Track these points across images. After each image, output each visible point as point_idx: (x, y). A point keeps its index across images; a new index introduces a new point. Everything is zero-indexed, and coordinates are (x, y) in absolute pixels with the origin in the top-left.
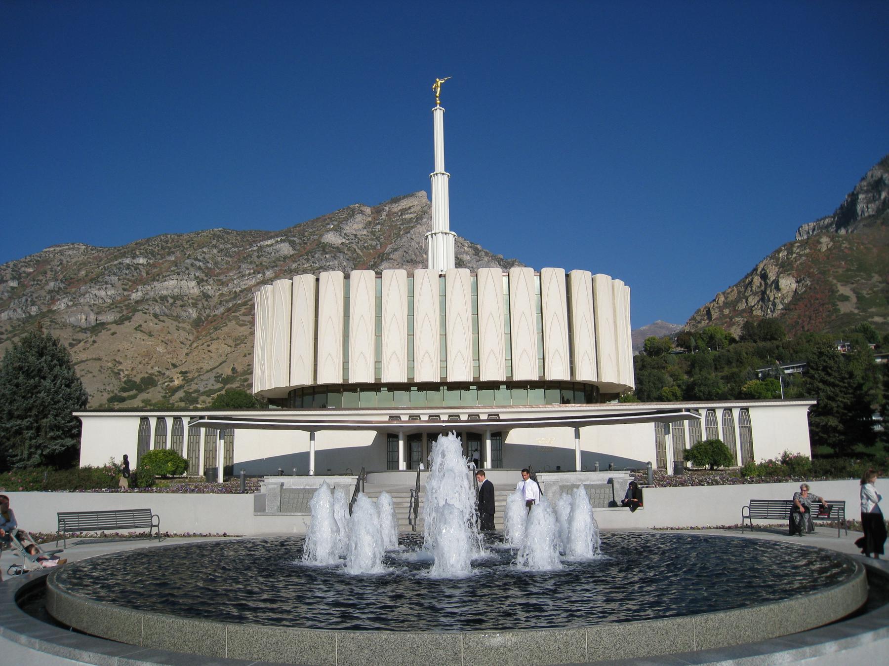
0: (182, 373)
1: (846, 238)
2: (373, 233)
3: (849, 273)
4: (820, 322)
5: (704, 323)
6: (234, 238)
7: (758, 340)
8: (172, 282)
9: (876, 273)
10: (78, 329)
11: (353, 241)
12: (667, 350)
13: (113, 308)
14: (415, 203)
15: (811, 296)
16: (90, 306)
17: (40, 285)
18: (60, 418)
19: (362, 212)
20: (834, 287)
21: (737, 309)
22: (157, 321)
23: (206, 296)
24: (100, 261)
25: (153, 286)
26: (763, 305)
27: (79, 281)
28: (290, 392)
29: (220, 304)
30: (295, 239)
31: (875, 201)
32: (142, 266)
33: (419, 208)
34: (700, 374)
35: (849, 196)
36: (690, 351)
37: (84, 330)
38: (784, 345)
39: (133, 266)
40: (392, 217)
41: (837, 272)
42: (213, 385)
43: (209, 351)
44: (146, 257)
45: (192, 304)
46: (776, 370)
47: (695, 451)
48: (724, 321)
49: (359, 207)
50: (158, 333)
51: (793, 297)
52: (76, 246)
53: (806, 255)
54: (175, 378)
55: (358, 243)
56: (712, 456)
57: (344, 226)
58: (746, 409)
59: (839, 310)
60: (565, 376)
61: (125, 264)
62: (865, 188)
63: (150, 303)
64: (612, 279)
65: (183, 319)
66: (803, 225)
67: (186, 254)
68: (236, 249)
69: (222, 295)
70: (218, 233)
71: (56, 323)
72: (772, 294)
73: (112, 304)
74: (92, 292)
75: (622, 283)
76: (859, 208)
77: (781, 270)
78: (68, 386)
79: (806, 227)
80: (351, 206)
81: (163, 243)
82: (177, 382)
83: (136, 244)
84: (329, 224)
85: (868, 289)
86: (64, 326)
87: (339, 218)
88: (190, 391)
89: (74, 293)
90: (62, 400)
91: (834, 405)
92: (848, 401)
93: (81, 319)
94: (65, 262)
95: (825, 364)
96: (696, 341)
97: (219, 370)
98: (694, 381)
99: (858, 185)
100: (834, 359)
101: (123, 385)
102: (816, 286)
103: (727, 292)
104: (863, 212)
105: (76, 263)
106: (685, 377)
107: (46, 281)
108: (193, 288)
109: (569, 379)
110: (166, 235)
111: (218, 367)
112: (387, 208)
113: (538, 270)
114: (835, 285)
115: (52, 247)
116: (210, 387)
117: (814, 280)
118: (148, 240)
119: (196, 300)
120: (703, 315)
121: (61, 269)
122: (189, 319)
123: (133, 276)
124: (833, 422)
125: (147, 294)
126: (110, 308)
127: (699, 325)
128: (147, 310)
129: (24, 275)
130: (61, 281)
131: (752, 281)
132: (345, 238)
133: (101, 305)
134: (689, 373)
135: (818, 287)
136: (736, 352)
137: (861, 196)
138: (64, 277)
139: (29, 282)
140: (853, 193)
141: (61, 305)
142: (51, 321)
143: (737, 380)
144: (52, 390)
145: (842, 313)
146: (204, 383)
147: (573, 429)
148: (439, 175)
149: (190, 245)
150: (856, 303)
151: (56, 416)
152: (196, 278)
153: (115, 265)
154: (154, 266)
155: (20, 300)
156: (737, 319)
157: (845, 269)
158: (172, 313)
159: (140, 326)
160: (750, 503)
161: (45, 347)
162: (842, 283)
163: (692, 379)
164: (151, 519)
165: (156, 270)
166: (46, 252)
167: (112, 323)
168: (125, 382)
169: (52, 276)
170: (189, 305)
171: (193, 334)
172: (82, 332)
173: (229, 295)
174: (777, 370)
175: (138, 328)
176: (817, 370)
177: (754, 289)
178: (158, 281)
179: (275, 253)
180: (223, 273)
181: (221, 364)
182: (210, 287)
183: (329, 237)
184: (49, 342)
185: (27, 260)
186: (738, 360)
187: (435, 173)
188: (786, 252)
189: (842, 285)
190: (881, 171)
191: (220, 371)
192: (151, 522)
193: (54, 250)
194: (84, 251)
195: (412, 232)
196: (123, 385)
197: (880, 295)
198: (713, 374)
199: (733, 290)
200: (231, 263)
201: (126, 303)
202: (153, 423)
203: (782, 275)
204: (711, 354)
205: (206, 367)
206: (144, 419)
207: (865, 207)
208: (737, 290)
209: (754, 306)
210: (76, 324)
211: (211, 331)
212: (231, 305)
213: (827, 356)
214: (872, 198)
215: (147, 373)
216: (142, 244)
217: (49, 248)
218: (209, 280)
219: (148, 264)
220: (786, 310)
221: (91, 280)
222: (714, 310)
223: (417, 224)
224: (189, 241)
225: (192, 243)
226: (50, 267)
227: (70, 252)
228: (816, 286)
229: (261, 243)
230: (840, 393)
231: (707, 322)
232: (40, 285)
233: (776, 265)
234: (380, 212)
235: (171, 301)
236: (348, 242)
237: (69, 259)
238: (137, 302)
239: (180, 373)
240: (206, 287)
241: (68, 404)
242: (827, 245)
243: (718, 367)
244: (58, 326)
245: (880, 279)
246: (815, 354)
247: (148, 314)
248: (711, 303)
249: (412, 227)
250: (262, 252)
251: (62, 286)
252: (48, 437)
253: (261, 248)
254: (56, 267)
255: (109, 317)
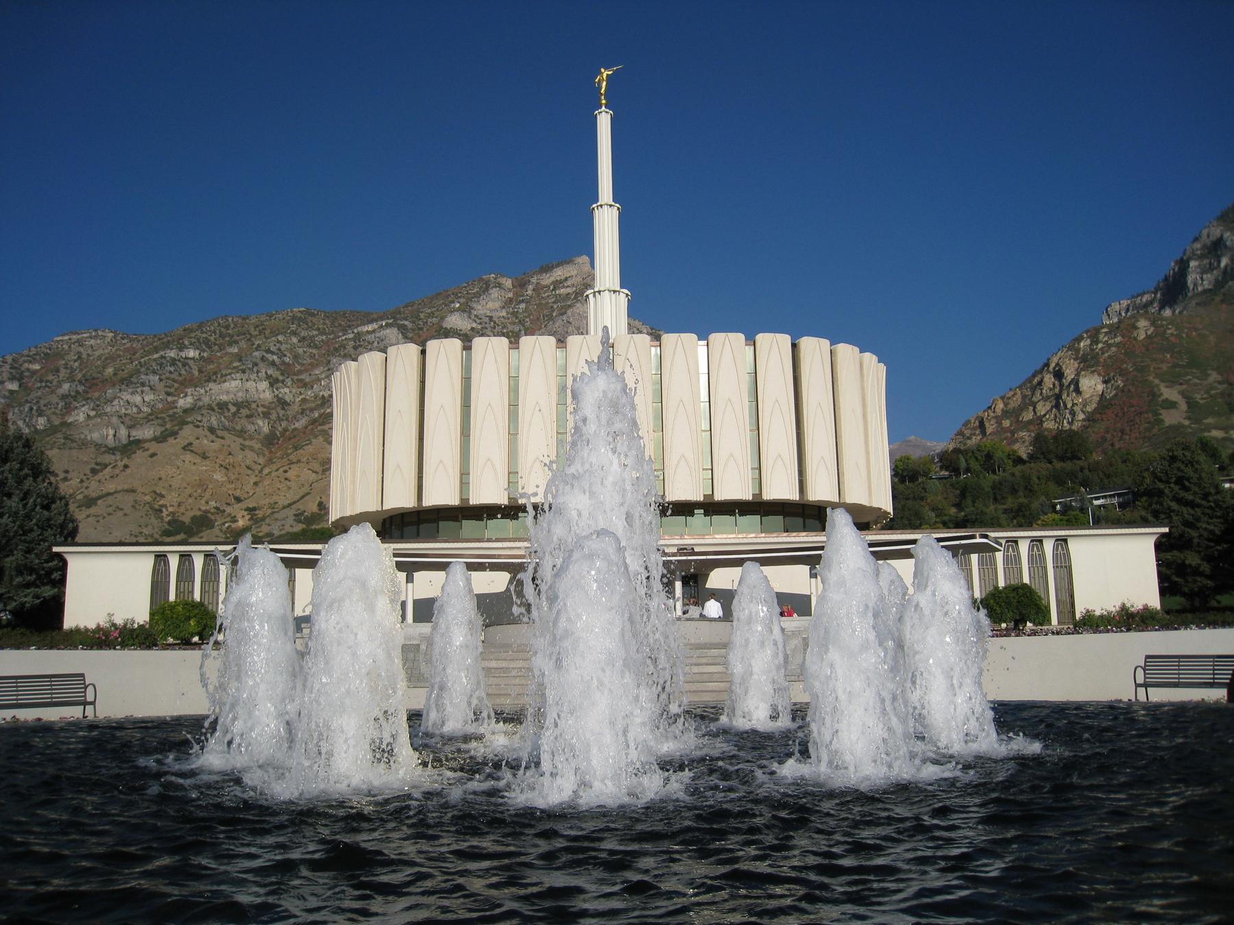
0: (248, 509)
1: (1171, 321)
2: (515, 314)
3: (1177, 370)
4: (1136, 438)
5: (975, 440)
6: (322, 321)
7: (1054, 460)
8: (234, 384)
9: (1213, 370)
10: (103, 449)
11: (487, 325)
12: (926, 474)
13: (152, 420)
14: (574, 273)
15: (1124, 402)
16: (121, 417)
17: (49, 387)
18: (33, 556)
19: (499, 286)
20: (1156, 389)
21: (1020, 419)
22: (213, 437)
23: (283, 403)
24: (134, 355)
25: (208, 389)
26: (1058, 415)
27: (104, 381)
28: (384, 520)
29: (302, 413)
30: (406, 323)
31: (1212, 270)
32: (192, 361)
33: (579, 279)
34: (973, 506)
35: (1176, 263)
36: (958, 473)
37: (112, 451)
38: (1091, 467)
39: (179, 360)
40: (542, 292)
41: (1159, 368)
42: (291, 526)
43: (286, 479)
44: (198, 349)
45: (263, 413)
46: (1081, 500)
47: (992, 601)
48: (1003, 437)
49: (495, 279)
50: (214, 454)
51: (1099, 403)
52: (100, 333)
53: (1117, 345)
54: (239, 516)
55: (494, 328)
56: (1017, 609)
57: (474, 305)
58: (1064, 540)
59: (1163, 420)
60: (792, 494)
61: (168, 359)
62: (1199, 252)
63: (204, 412)
64: (861, 352)
65: (250, 435)
66: (1113, 304)
67: (254, 344)
68: (324, 337)
69: (304, 400)
70: (299, 315)
71: (73, 441)
72: (1069, 399)
73: (150, 414)
74: (123, 397)
75: (875, 358)
76: (1190, 279)
77: (1082, 365)
78: (47, 507)
79: (1116, 306)
80: (484, 277)
81: (222, 329)
82: (241, 523)
83: (184, 330)
84: (453, 302)
85: (1202, 392)
86: (83, 444)
87: (468, 293)
88: (260, 534)
89: (98, 399)
90: (35, 528)
91: (1194, 534)
92: (1216, 528)
93: (107, 434)
94: (84, 356)
95: (1180, 474)
96: (966, 461)
97: (300, 506)
98: (966, 516)
99: (1188, 248)
100: (1193, 466)
101: (167, 527)
102: (1131, 387)
103: (1007, 395)
104: (1195, 285)
105: (99, 358)
106: (953, 511)
107: (58, 381)
108: (264, 391)
109: (798, 499)
110: (226, 318)
111: (298, 501)
112: (534, 280)
113: (751, 340)
114: (1157, 386)
115: (67, 334)
116: (288, 529)
117: (1127, 380)
118: (201, 326)
119: (269, 408)
120: (974, 429)
121: (80, 365)
122: (259, 434)
123: (180, 375)
124: (1192, 559)
125: (199, 399)
126: (148, 419)
127: (969, 442)
128: (200, 421)
129: (26, 374)
130: (80, 382)
131: (1042, 380)
132: (475, 321)
133: (136, 416)
134: (958, 506)
135: (1133, 389)
136: (1023, 477)
137: (1193, 264)
138: (84, 376)
139: (34, 384)
140: (1182, 259)
141: (80, 416)
142: (66, 438)
143: (1027, 513)
144: (21, 513)
145: (1167, 424)
146: (279, 523)
147: (807, 568)
148: (605, 208)
149: (260, 332)
150: (1186, 412)
151: (29, 551)
152: (268, 377)
153: (155, 360)
154: (209, 361)
155: (22, 409)
156: (1022, 434)
157: (1170, 365)
158: (235, 426)
159: (191, 444)
160: (1146, 662)
161: (11, 450)
162: (1167, 384)
163: (963, 514)
164: (85, 692)
165: (211, 367)
166: (58, 341)
167: (150, 441)
168: (169, 523)
169: (67, 376)
170: (259, 415)
171: (264, 455)
172: (109, 453)
173: (313, 402)
174: (1082, 500)
175: (187, 447)
176: (1168, 482)
177: (1044, 391)
178: (215, 381)
179: (378, 343)
180: (306, 370)
181: (303, 497)
182: (287, 390)
183: (454, 319)
184: (17, 442)
185: (31, 353)
186: (1026, 488)
187: (599, 204)
188: (1089, 340)
189: (1167, 387)
190: (1221, 228)
191: (301, 507)
192: (85, 696)
193: (70, 339)
194: (112, 340)
195: (569, 312)
196: (167, 527)
197: (1220, 400)
198: (992, 507)
199: (1015, 394)
200: (317, 357)
201: (171, 412)
202: (174, 562)
203: (1083, 373)
204: (989, 479)
205: (283, 501)
206: (161, 558)
207: (1198, 279)
208: (1022, 393)
209: (1045, 415)
210: (100, 442)
211: (289, 451)
212: (317, 415)
213: (1183, 462)
214: (1208, 266)
215: (200, 509)
216: (191, 331)
217: (62, 335)
218: (287, 380)
219: (201, 358)
220: (1089, 421)
221: (122, 381)
222: (990, 421)
223: (577, 302)
224: (257, 326)
225: (263, 329)
226: (63, 362)
227: (92, 342)
228: (1131, 387)
229: (359, 329)
230: (1202, 516)
231: (979, 438)
232: (49, 387)
233: (1075, 359)
234: (524, 285)
235: (233, 409)
236: (479, 327)
237: (90, 352)
238: (186, 411)
239: (245, 510)
240: (282, 390)
241: (46, 534)
242: (1146, 330)
243: (999, 497)
244: (74, 444)
245: (1219, 378)
246: (1164, 459)
247: (201, 428)
248: (984, 411)
249: (570, 306)
250: (360, 341)
251: (81, 388)
252: (14, 583)
253: (358, 336)
254: (72, 363)
255: (146, 432)
